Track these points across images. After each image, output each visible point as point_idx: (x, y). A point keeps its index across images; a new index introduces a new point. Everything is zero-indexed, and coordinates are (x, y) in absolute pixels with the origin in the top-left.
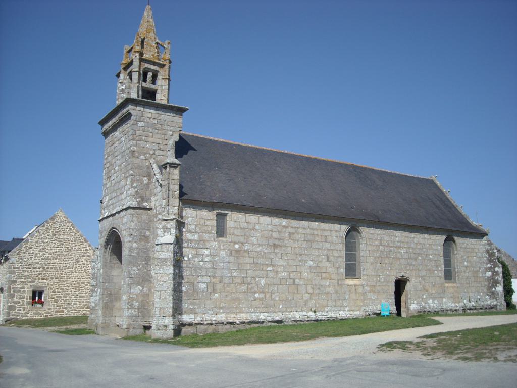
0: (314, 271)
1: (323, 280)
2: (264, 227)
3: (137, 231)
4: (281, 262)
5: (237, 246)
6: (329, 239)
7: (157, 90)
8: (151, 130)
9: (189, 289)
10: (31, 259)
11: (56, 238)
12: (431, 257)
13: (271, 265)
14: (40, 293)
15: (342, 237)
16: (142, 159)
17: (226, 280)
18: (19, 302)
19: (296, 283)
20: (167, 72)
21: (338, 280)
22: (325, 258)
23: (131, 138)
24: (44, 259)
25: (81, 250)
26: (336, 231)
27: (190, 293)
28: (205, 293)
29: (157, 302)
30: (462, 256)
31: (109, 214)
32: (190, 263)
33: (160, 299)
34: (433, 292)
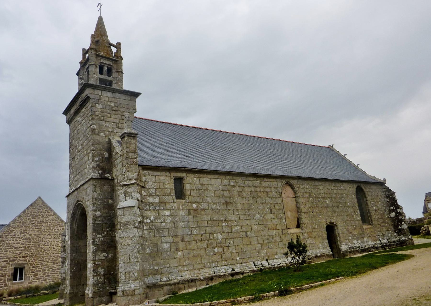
4: (233, 217)
5: (194, 206)
6: (270, 194)
7: (112, 81)
8: (108, 111)
9: (153, 250)
12: (349, 204)
14: (22, 270)
17: (187, 239)
19: (248, 235)
21: (282, 230)
22: (269, 211)
23: (90, 118)
24: (25, 239)
25: (58, 229)
26: (275, 187)
28: (168, 253)
31: (75, 189)
32: (152, 225)
33: (125, 263)
34: (356, 233)
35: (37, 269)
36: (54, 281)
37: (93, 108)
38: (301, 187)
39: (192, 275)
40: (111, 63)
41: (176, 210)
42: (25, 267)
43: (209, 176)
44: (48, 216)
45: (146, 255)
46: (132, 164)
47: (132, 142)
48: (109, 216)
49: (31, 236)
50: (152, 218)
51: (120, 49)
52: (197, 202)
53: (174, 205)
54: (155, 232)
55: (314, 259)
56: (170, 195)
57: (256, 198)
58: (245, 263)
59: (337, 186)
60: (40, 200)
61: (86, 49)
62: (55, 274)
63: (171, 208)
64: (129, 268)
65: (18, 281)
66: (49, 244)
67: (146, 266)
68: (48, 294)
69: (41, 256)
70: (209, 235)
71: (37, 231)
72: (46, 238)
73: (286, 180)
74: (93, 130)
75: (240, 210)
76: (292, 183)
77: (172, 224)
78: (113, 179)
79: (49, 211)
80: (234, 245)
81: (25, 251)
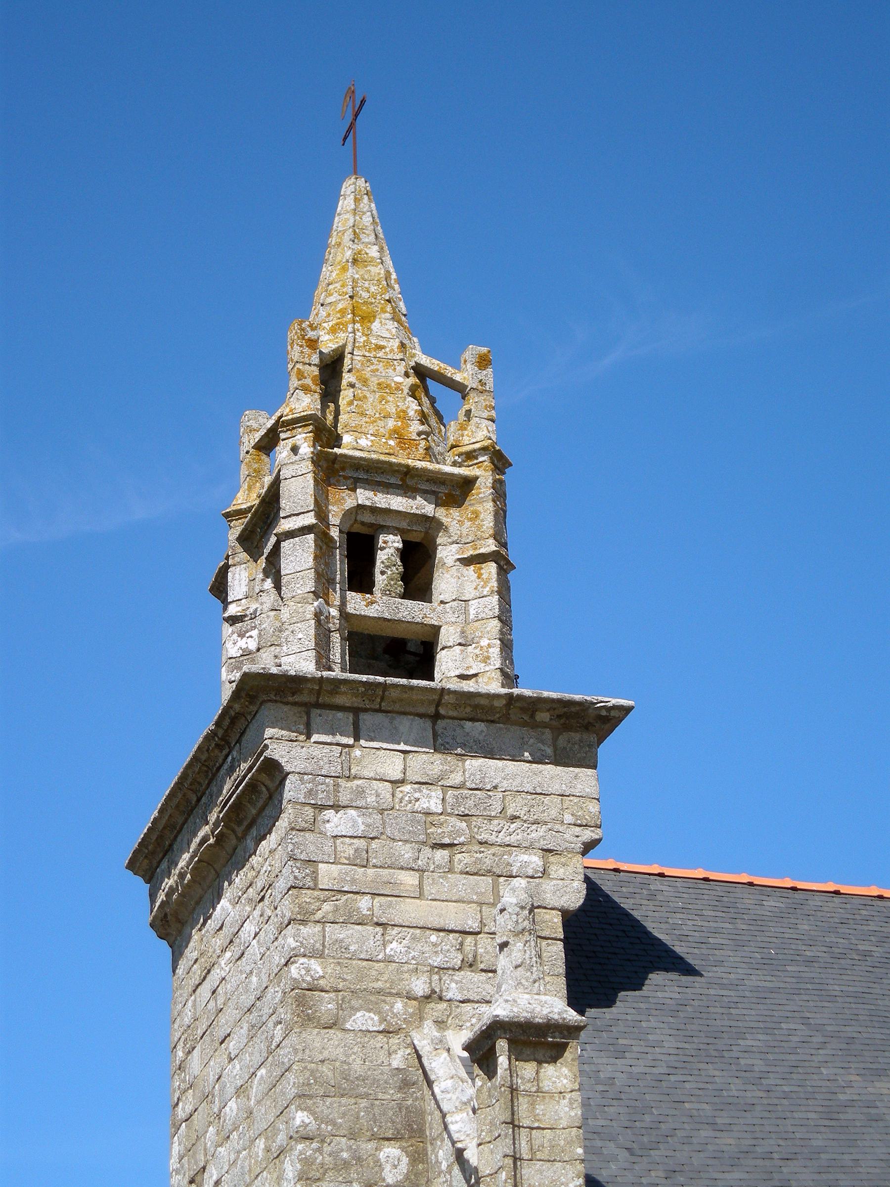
7: (436, 629)
8: (406, 852)
20: (488, 522)
40: (421, 506)
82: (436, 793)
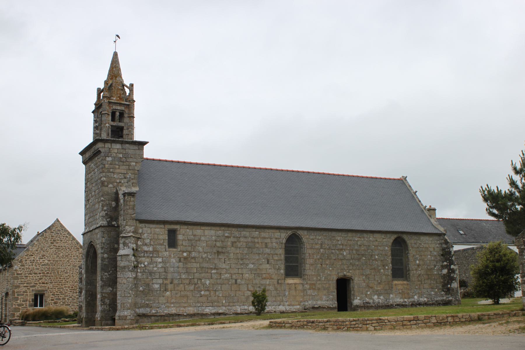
0: (255, 273)
1: (264, 280)
2: (208, 238)
3: (107, 244)
4: (224, 266)
5: (185, 254)
6: (270, 245)
7: (123, 127)
8: (117, 163)
10: (33, 266)
11: (54, 246)
13: (215, 268)
14: (42, 296)
15: (282, 243)
16: (111, 187)
17: (176, 282)
18: (23, 305)
22: (265, 261)
24: (44, 265)
25: (77, 256)
26: (276, 238)
27: (146, 292)
28: (158, 292)
29: (119, 299)
30: (414, 255)
31: (89, 230)
32: (146, 269)
33: (121, 296)
35: (56, 297)
36: (74, 311)
37: (103, 161)
38: (312, 237)
39: (178, 311)
40: (123, 108)
41: (167, 258)
42: (44, 294)
43: (203, 228)
44: (67, 240)
45: (139, 292)
46: (130, 219)
47: (131, 200)
48: (114, 258)
49: (50, 262)
50: (146, 263)
51: (133, 91)
52: (188, 251)
53: (166, 254)
54: (147, 275)
55: (311, 310)
56: (163, 245)
57: (252, 249)
58: (231, 306)
59: (363, 237)
60: (57, 222)
61: (100, 88)
62: (75, 304)
63: (163, 256)
64: (124, 300)
65: (38, 307)
66: (68, 271)
67: (139, 300)
68: (68, 321)
69: (60, 283)
70: (197, 280)
71: (56, 257)
72: (65, 265)
73: (293, 231)
74: (103, 183)
75: (232, 260)
76: (300, 233)
77: (163, 269)
78: (118, 227)
79: (68, 236)
80: (221, 290)
81: (45, 277)
82: (122, 155)
